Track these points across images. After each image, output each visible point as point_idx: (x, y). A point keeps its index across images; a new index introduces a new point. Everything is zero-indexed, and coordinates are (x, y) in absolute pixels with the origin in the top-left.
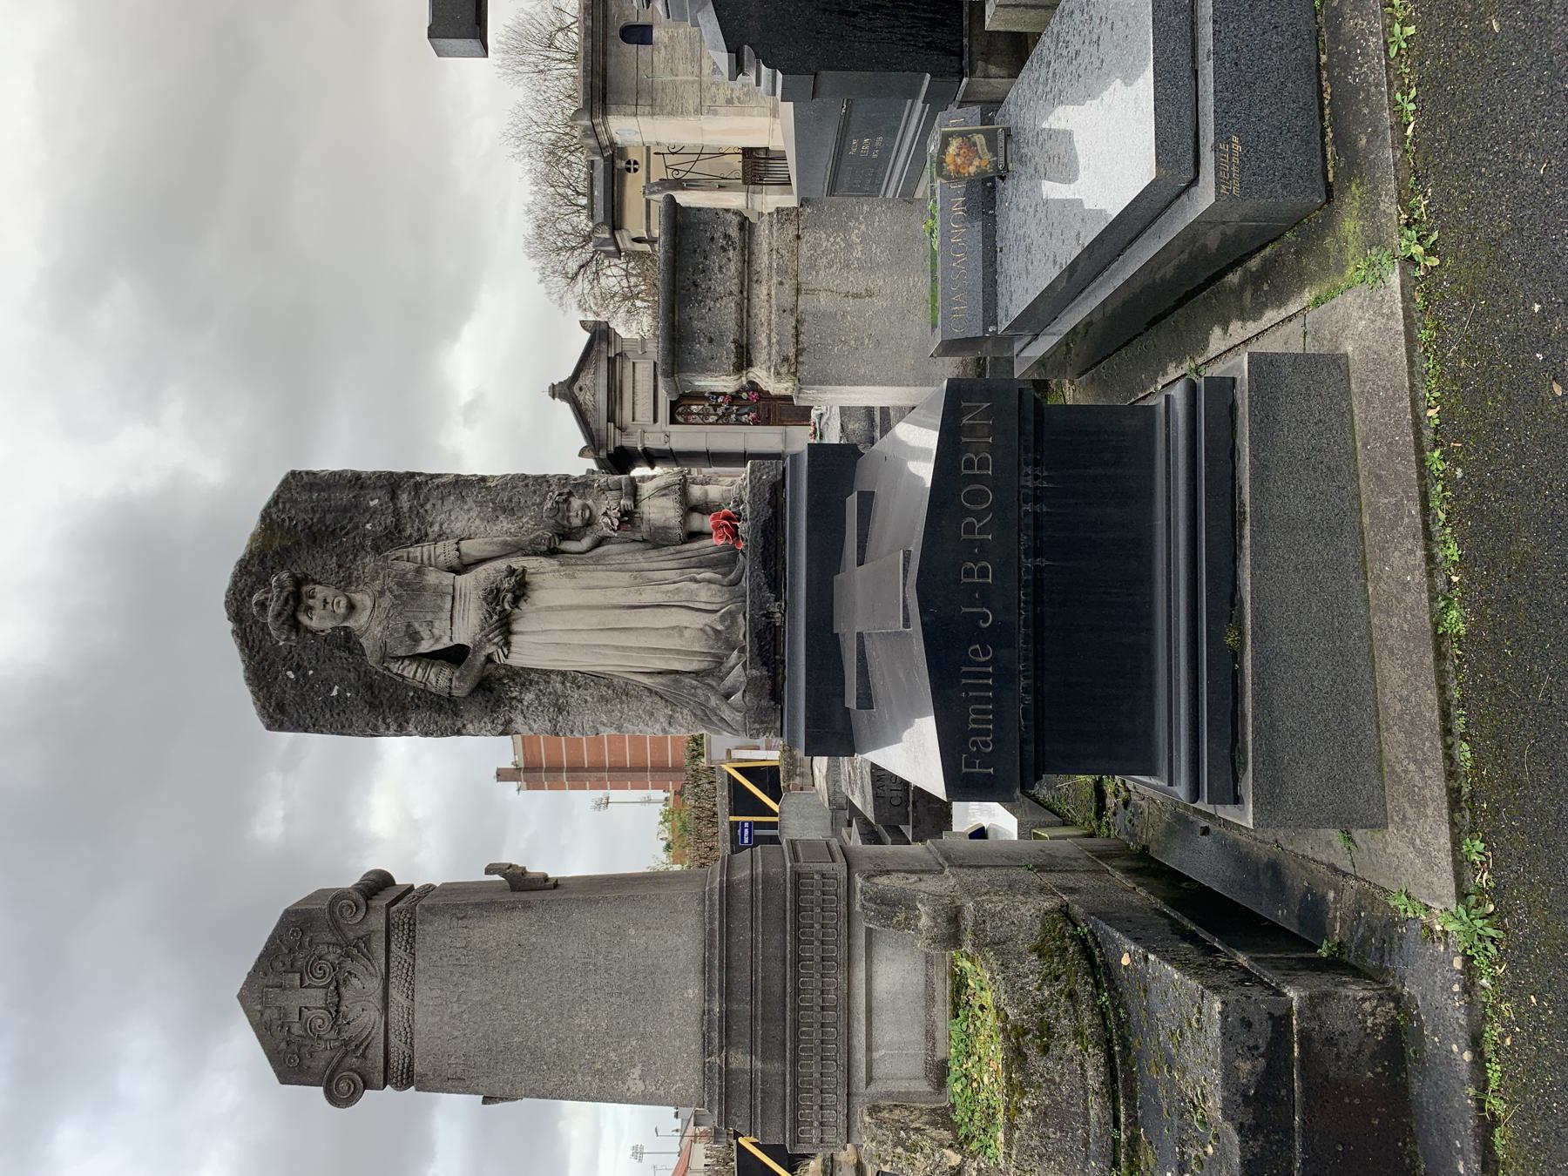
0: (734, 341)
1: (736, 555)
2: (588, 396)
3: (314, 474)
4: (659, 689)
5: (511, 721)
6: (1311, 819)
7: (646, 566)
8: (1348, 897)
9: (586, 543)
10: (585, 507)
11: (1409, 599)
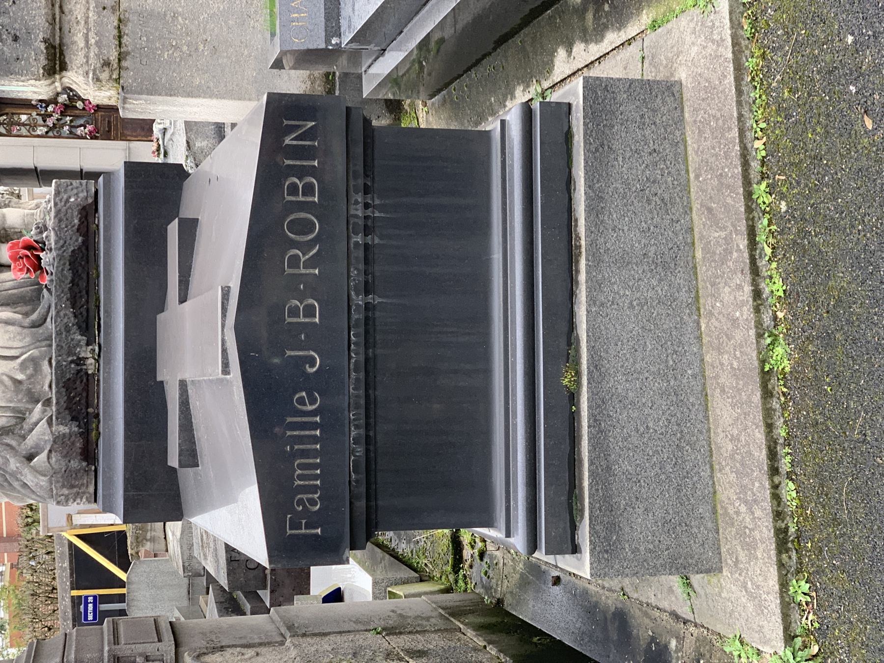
0: (45, 41)
1: (40, 290)
6: (650, 566)
8: (689, 645)
11: (738, 335)
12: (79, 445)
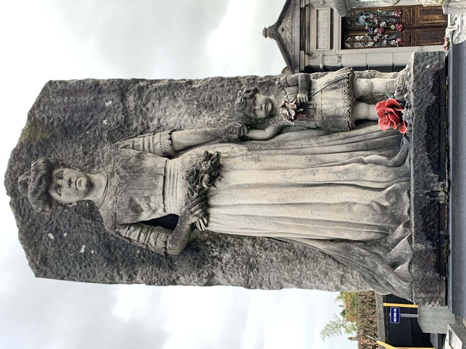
2: (288, 34)
3: (65, 83)
4: (331, 253)
5: (213, 275)
7: (319, 149)
9: (269, 131)
10: (268, 101)
12: (433, 259)
